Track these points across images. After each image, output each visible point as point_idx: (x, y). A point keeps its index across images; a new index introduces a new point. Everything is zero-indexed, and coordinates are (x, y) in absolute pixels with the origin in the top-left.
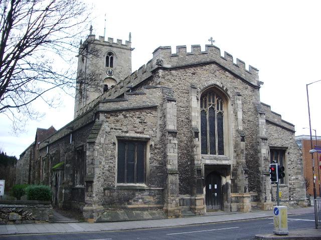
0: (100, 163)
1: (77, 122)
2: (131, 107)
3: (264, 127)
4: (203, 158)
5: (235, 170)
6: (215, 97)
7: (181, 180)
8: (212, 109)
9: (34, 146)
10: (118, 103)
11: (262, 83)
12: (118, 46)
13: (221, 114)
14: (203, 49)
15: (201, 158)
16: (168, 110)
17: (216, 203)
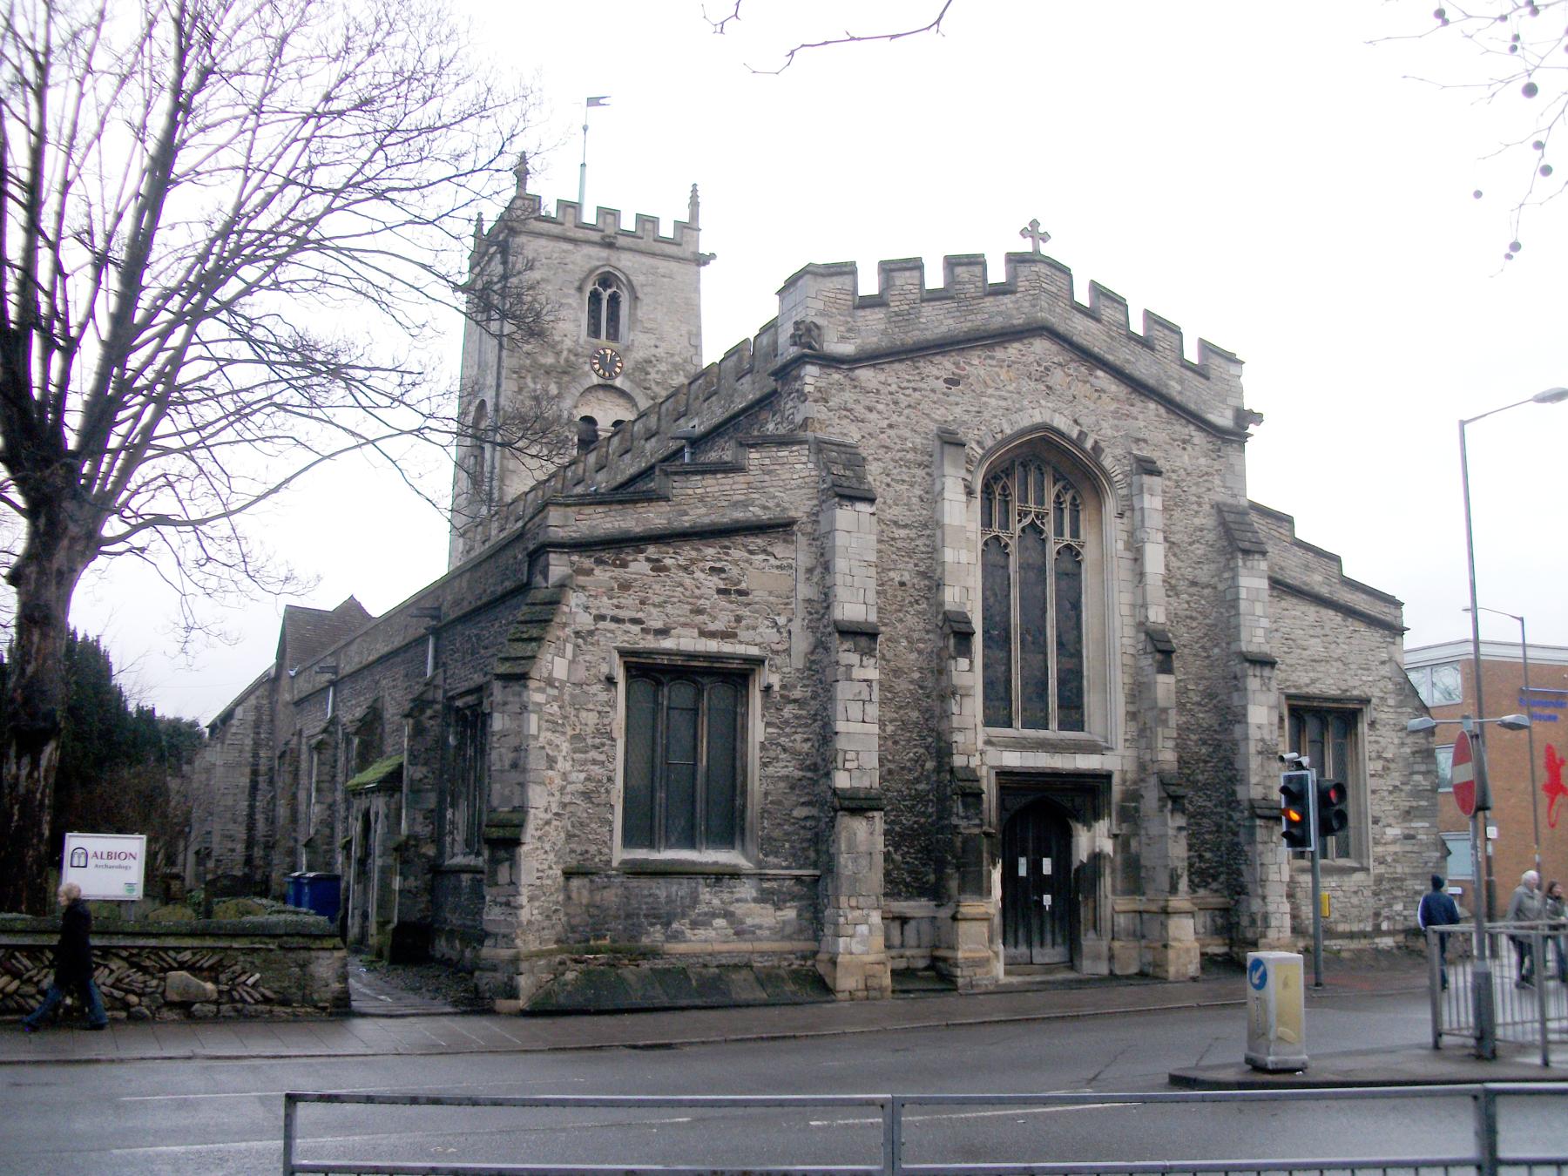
0: (551, 762)
1: (456, 583)
2: (686, 522)
3: (1259, 609)
4: (988, 742)
5: (1133, 795)
6: (1048, 482)
7: (895, 838)
8: (1035, 529)
9: (269, 683)
10: (630, 509)
11: (1257, 418)
12: (641, 244)
13: (1072, 553)
14: (997, 273)
15: (980, 745)
16: (841, 539)
17: (1048, 937)
